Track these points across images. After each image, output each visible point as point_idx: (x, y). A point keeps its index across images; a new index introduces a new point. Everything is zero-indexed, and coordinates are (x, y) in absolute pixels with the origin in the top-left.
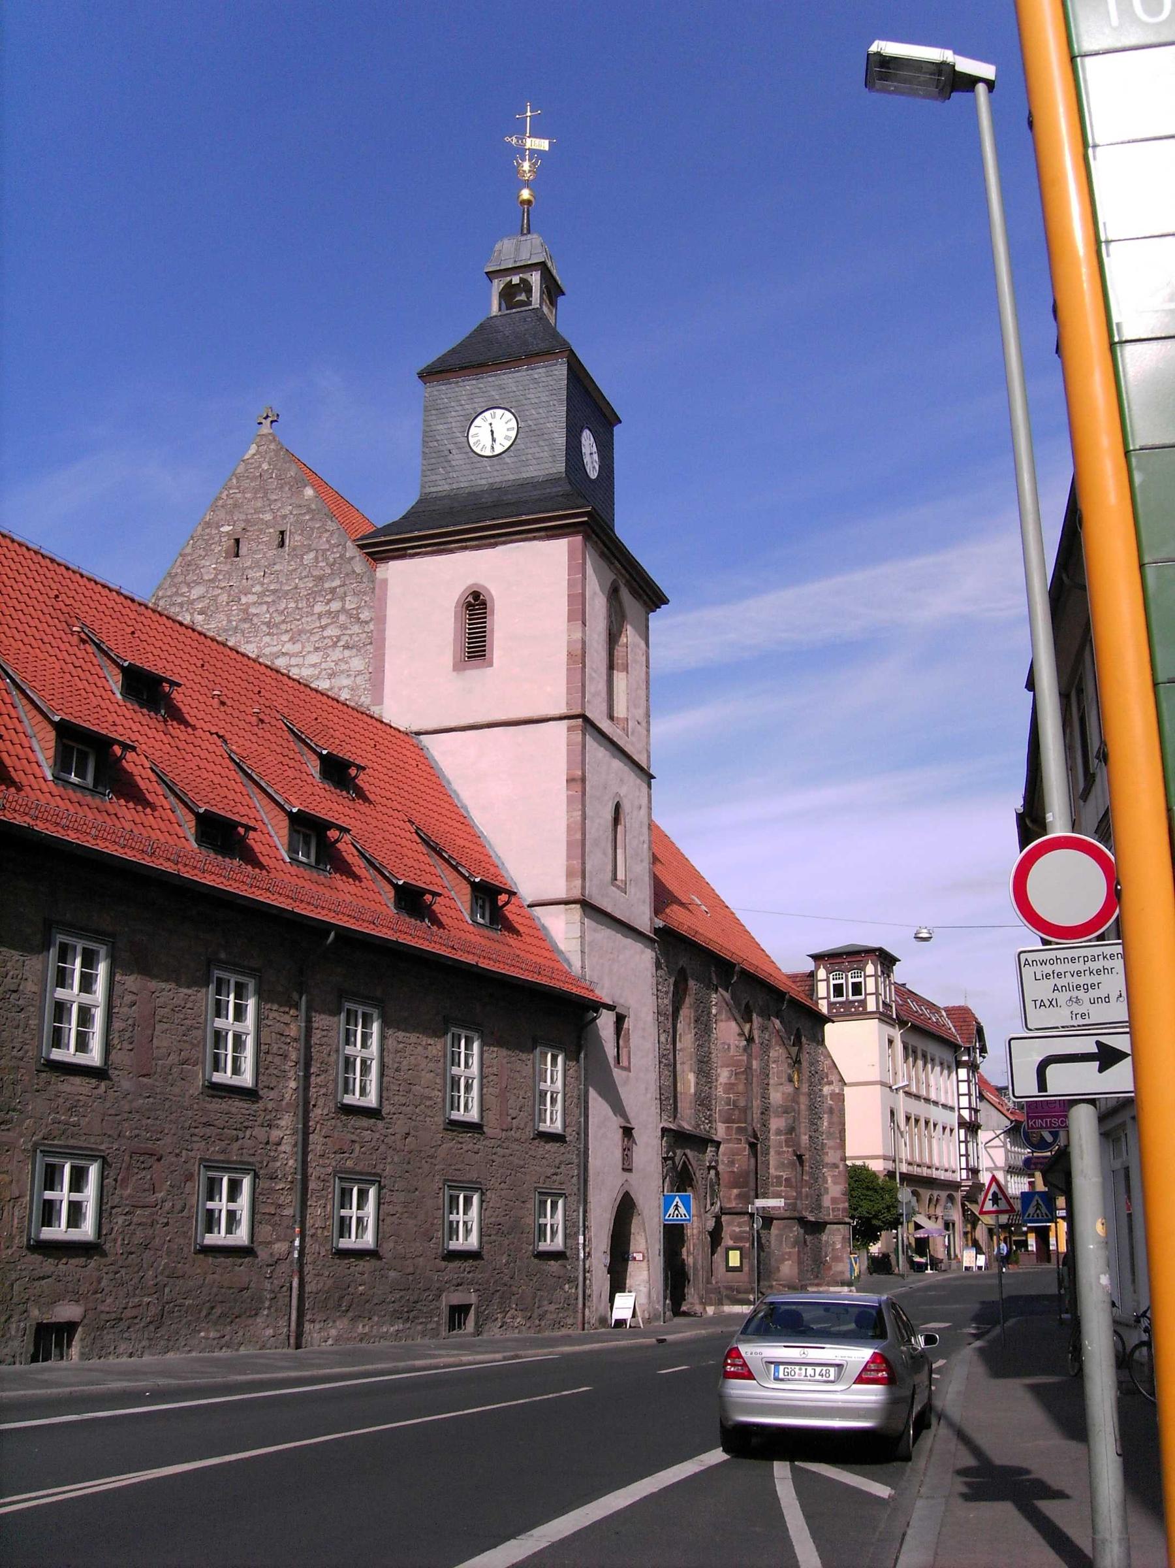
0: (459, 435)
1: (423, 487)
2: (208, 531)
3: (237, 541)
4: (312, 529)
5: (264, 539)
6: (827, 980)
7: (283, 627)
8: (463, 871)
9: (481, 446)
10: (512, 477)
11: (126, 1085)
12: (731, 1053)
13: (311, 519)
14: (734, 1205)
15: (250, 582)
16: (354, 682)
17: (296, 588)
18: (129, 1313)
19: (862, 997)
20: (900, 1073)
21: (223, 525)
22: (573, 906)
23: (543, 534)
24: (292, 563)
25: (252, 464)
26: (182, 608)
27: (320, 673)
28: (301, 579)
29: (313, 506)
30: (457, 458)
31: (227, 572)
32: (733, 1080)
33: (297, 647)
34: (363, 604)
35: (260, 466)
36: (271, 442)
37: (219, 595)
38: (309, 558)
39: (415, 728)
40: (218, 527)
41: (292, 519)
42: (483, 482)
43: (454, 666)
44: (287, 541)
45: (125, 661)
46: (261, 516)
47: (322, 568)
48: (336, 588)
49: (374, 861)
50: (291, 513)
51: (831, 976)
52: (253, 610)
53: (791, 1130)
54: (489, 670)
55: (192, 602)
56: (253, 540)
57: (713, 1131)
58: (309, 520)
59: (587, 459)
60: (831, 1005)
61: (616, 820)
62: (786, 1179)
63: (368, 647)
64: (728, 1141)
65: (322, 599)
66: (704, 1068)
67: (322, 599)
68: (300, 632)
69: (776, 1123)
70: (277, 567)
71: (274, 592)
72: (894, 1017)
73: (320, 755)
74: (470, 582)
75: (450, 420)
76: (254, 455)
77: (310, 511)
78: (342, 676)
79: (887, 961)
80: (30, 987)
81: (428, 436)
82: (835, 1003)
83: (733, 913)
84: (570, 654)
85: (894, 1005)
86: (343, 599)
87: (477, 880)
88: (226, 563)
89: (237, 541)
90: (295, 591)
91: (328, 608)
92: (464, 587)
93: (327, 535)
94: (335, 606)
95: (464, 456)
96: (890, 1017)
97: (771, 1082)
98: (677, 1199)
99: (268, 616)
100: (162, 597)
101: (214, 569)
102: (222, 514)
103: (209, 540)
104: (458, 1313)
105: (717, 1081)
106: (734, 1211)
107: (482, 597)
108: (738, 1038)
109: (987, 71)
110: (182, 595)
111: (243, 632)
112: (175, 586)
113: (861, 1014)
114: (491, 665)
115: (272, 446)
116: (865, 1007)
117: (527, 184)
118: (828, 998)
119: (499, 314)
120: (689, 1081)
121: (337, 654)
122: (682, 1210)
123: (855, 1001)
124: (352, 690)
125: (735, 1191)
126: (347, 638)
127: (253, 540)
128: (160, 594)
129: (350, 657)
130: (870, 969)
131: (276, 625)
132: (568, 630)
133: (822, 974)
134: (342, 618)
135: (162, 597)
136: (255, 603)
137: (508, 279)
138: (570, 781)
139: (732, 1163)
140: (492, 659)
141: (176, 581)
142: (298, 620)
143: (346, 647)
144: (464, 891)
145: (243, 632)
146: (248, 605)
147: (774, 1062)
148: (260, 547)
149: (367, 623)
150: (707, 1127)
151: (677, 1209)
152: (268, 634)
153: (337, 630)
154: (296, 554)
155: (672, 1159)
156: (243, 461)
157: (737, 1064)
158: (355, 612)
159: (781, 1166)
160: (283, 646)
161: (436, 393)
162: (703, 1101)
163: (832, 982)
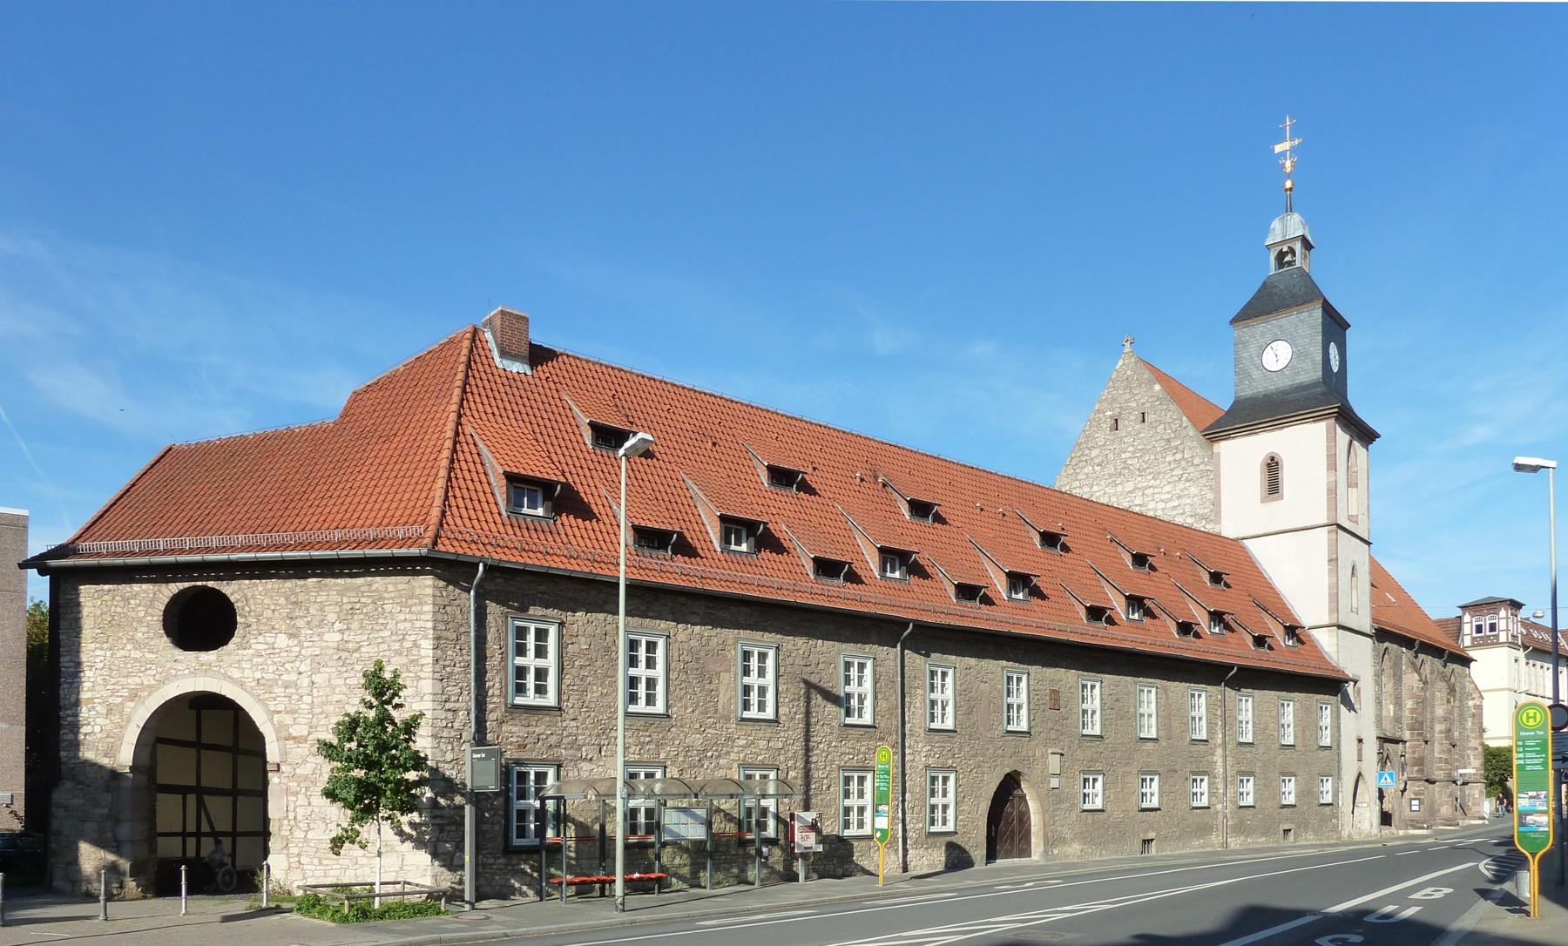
1: (1236, 393)
6: (1471, 622)
7: (1148, 471)
11: (1164, 744)
18: (1170, 834)
19: (1496, 633)
20: (1523, 680)
22: (1332, 628)
29: (1161, 396)
30: (1256, 374)
32: (1415, 706)
39: (1241, 536)
42: (1273, 387)
43: (1261, 499)
44: (1146, 419)
51: (1474, 619)
52: (1129, 462)
53: (1449, 731)
55: (1092, 459)
60: (1474, 639)
64: (1411, 740)
66: (1398, 703)
68: (1159, 473)
69: (1438, 727)
70: (1142, 435)
71: (1141, 450)
72: (1520, 644)
79: (1516, 605)
80: (1132, 709)
81: (1237, 361)
82: (1476, 638)
84: (1328, 490)
85: (1519, 636)
86: (1183, 452)
88: (1110, 435)
89: (1116, 420)
93: (1171, 413)
94: (1179, 456)
95: (1259, 372)
96: (1517, 645)
104: (1287, 831)
109: (1552, 464)
110: (1086, 455)
111: (1124, 475)
113: (1496, 644)
114: (1282, 499)
116: (1498, 639)
117: (1289, 176)
118: (1471, 634)
120: (1390, 710)
121: (1181, 486)
122: (1389, 780)
123: (1490, 636)
125: (1416, 768)
130: (1503, 613)
131: (1144, 470)
132: (1327, 475)
133: (1467, 618)
137: (1280, 248)
138: (1330, 560)
139: (1414, 752)
143: (1187, 480)
145: (1124, 475)
146: (1126, 459)
152: (1140, 476)
154: (1152, 426)
155: (1382, 753)
159: (1442, 751)
162: (1397, 719)
163: (1475, 624)
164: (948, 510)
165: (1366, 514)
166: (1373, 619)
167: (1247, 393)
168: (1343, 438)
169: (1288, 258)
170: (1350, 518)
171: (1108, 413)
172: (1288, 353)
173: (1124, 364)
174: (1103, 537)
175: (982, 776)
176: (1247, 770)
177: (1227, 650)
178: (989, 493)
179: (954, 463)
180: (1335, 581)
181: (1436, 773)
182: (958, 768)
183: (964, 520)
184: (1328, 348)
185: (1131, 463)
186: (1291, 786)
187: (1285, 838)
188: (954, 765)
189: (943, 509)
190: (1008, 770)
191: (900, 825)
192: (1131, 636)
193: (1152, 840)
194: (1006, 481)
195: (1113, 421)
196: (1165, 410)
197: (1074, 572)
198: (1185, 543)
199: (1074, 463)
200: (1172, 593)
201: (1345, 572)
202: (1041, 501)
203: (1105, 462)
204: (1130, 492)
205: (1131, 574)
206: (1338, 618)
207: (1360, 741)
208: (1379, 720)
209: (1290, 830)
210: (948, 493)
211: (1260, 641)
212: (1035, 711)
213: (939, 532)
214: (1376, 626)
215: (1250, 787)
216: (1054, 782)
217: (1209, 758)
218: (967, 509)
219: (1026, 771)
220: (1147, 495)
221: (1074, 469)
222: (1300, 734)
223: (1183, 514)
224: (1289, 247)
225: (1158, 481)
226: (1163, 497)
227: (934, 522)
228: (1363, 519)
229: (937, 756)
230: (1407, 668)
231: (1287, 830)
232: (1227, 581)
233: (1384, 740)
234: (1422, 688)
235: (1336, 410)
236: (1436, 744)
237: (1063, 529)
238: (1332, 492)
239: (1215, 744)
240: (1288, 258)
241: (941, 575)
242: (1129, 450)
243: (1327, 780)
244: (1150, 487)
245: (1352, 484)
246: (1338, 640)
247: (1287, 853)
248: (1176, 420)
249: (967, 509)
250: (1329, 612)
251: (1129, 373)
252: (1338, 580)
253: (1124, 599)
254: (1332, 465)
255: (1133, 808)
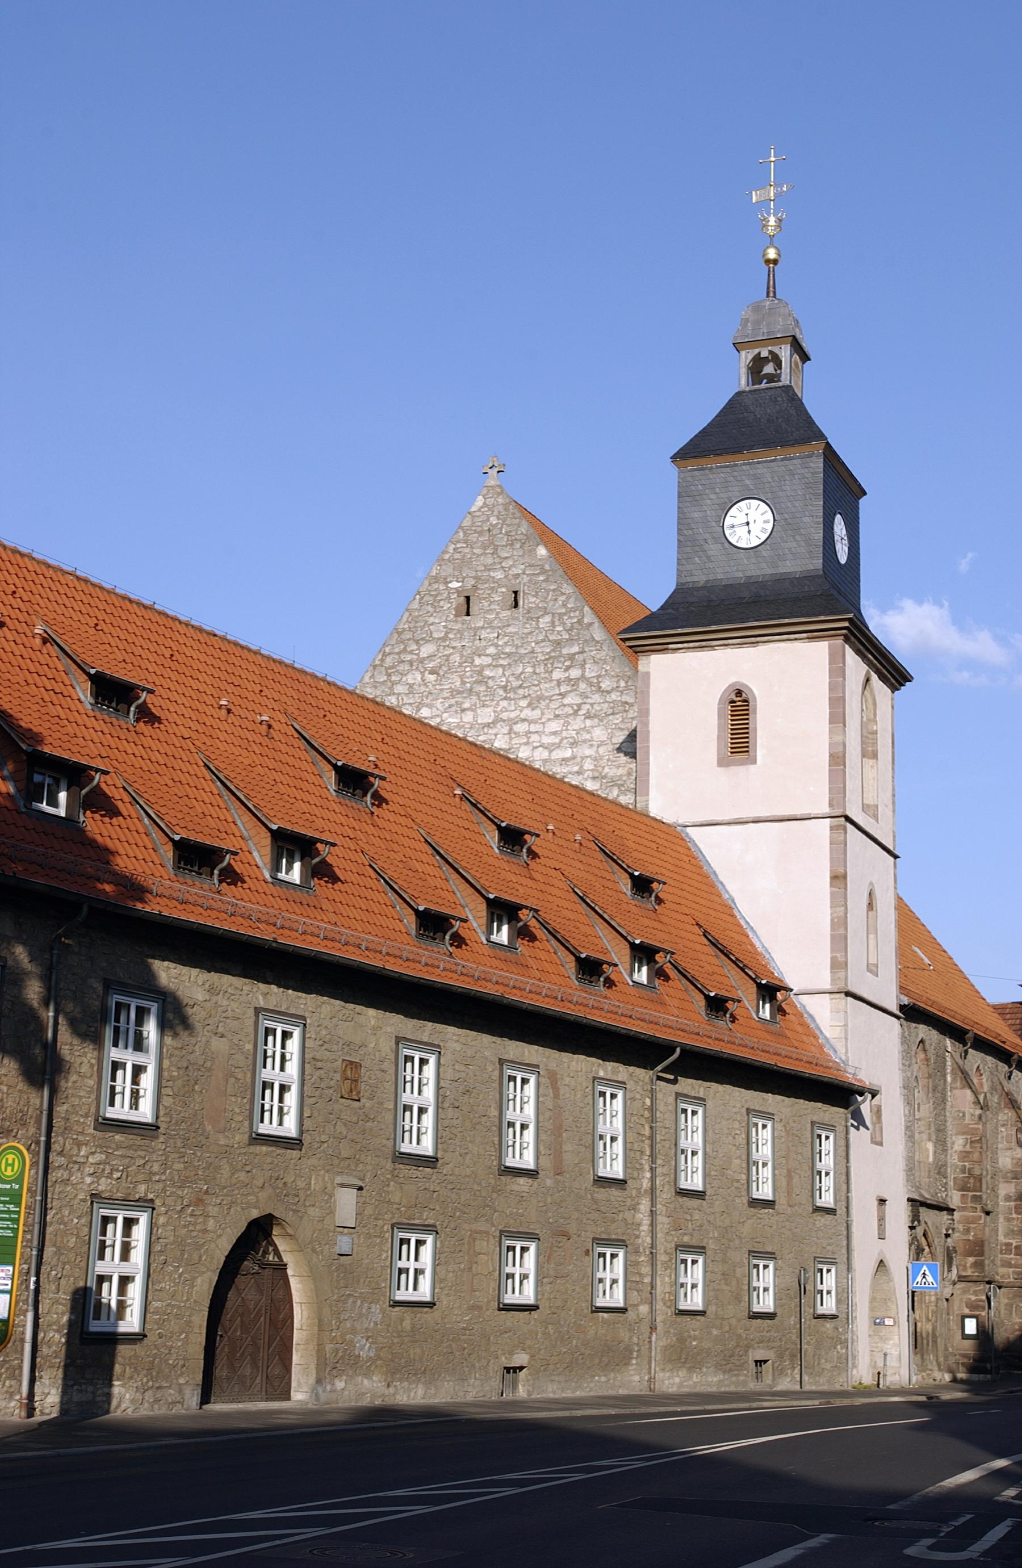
0: (714, 524)
2: (436, 586)
3: (468, 598)
4: (547, 591)
5: (497, 599)
7: (521, 692)
8: (750, 973)
9: (736, 537)
10: (769, 571)
11: (549, 1182)
12: (966, 1122)
13: (546, 581)
14: (969, 1273)
15: (483, 643)
16: (597, 752)
17: (533, 652)
21: (451, 582)
23: (805, 635)
24: (528, 626)
25: (479, 517)
26: (412, 666)
27: (561, 741)
28: (537, 643)
29: (547, 567)
30: (714, 549)
31: (459, 631)
32: (968, 1148)
33: (537, 713)
34: (604, 673)
35: (488, 520)
36: (499, 494)
37: (450, 654)
38: (545, 621)
40: (446, 583)
41: (526, 579)
44: (521, 603)
45: (503, 822)
46: (492, 574)
47: (559, 632)
48: (574, 654)
49: (686, 974)
50: (524, 573)
52: (487, 673)
54: (752, 768)
55: (422, 661)
56: (484, 598)
57: (949, 1199)
58: (543, 581)
59: (838, 546)
61: (871, 906)
62: (1016, 1247)
63: (611, 717)
64: (964, 1209)
65: (560, 665)
66: (942, 1144)
67: (560, 665)
68: (540, 698)
70: (511, 629)
71: (509, 655)
73: (632, 876)
74: (733, 680)
75: (705, 508)
76: (482, 507)
77: (543, 571)
78: (585, 745)
83: (951, 958)
86: (583, 666)
87: (764, 982)
88: (456, 621)
89: (468, 598)
90: (532, 655)
91: (567, 675)
92: (727, 686)
93: (563, 598)
94: (575, 673)
97: (1000, 1146)
98: (925, 1268)
99: (504, 679)
100: (390, 654)
101: (445, 627)
102: (448, 570)
103: (436, 596)
105: (952, 1148)
106: (970, 1279)
107: (744, 695)
108: (972, 1106)
110: (411, 652)
111: (478, 694)
112: (402, 642)
115: (500, 500)
117: (771, 241)
119: (747, 389)
120: (927, 1150)
121: (577, 723)
122: (930, 1279)
124: (595, 761)
125: (971, 1260)
126: (588, 706)
127: (484, 598)
128: (387, 649)
129: (592, 727)
131: (514, 690)
134: (583, 686)
135: (390, 654)
136: (489, 665)
137: (756, 351)
139: (967, 1231)
140: (756, 756)
141: (403, 637)
142: (536, 685)
143: (588, 716)
144: (750, 991)
145: (478, 694)
146: (483, 667)
147: (1003, 1125)
148: (493, 607)
149: (608, 692)
150: (944, 1195)
151: (924, 1277)
152: (505, 698)
153: (577, 698)
156: (469, 513)
157: (972, 1132)
158: (596, 681)
160: (521, 711)
161: (689, 479)
162: (940, 1170)
164: (166, 704)
165: (891, 806)
166: (901, 987)
167: (696, 579)
168: (855, 666)
169: (769, 369)
170: (865, 808)
171: (455, 585)
172: (766, 522)
173: (485, 505)
174: (446, 790)
175: (205, 1222)
176: (694, 1242)
177: (662, 1017)
178: (245, 684)
179: (180, 622)
180: (89, 1220)
181: (1002, 1271)
182: (158, 1203)
183: (194, 726)
184: (833, 523)
185: (491, 675)
186: (766, 1278)
187: (758, 1376)
188: (151, 1196)
189: (158, 701)
190: (255, 1214)
191: (30, 1316)
192: (497, 974)
193: (521, 1368)
194: (277, 668)
195: (462, 600)
196: (554, 590)
197: (395, 847)
198: (589, 820)
199: (389, 661)
200: (566, 904)
201: (857, 903)
202: (339, 711)
203: (445, 668)
204: (488, 725)
205: (497, 863)
206: (846, 978)
207: (882, 1201)
208: (911, 1169)
209: (765, 1361)
210: (167, 673)
211: (717, 1005)
212: (312, 1100)
213: (148, 742)
214: (905, 1001)
215: (696, 1273)
216: (344, 1243)
217: (628, 1215)
218: (202, 708)
219: (290, 1217)
220: (517, 734)
221: (389, 675)
222: (784, 1182)
223: (578, 773)
224: (770, 352)
225: (538, 712)
226: (546, 740)
227: (137, 720)
228: (885, 812)
229: (116, 1175)
230: (954, 1080)
231: (761, 1361)
232: (660, 895)
233: (916, 1204)
234: (980, 1117)
235: (846, 624)
236: (1001, 1220)
237: (376, 766)
238: (837, 760)
239: (639, 1190)
240: (769, 369)
241: (146, 820)
242: (488, 652)
243: (829, 1271)
244: (524, 720)
245: (869, 752)
246: (846, 1019)
247: (766, 1404)
248: (571, 610)
249: (202, 708)
250: (832, 968)
251: (493, 520)
252: (846, 914)
253: (484, 906)
254: (837, 717)
255: (489, 1302)
